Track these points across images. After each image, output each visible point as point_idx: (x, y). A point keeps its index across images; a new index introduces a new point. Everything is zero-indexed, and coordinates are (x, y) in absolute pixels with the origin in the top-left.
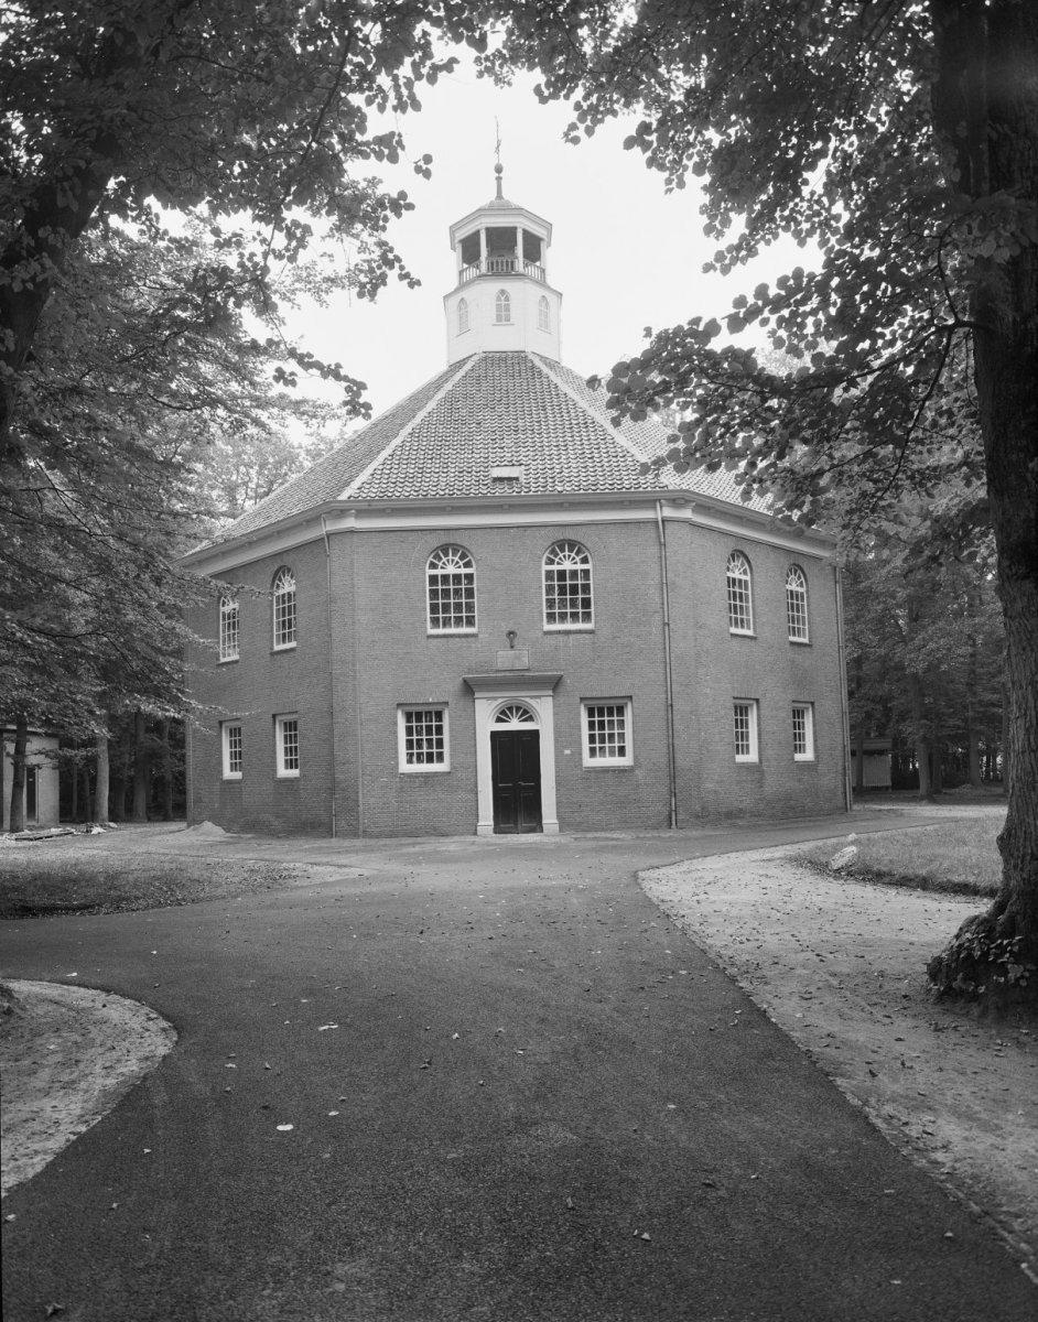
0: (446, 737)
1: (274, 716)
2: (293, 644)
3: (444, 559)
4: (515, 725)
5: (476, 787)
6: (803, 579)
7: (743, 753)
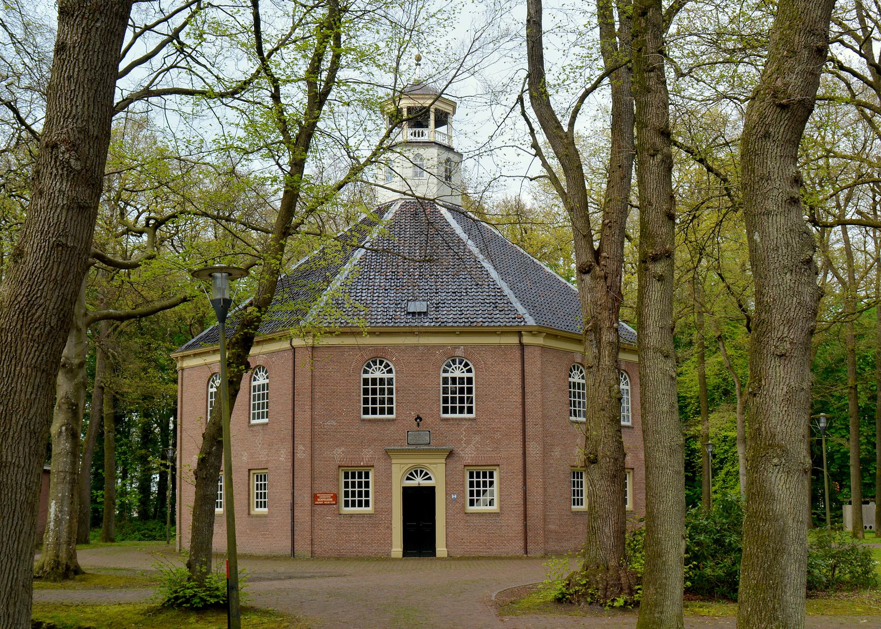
0: (371, 489)
1: (249, 470)
2: (266, 420)
3: (374, 367)
4: (418, 481)
6: (628, 379)
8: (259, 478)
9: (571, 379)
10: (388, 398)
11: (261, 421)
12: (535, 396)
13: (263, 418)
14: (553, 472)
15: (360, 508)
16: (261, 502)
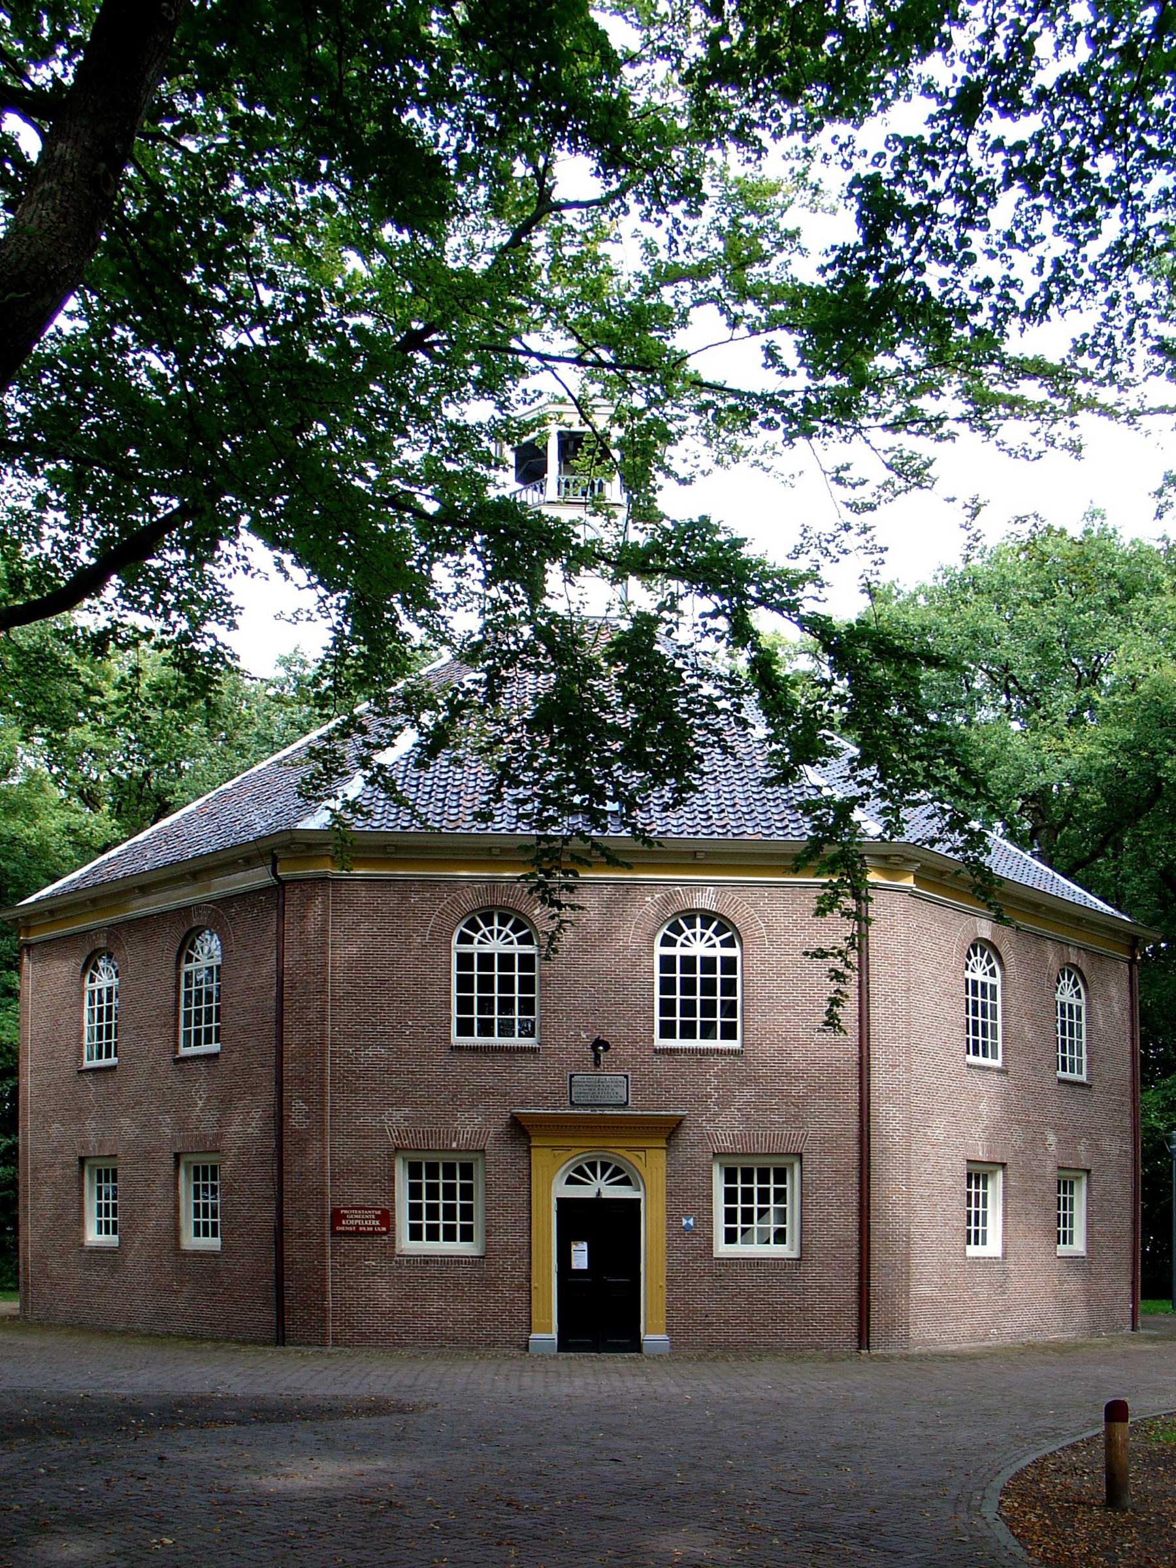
2: (214, 1047)
5: (530, 1281)
6: (1080, 986)
7: (976, 1243)
8: (200, 1172)
9: (969, 975)
10: (512, 1013)
11: (204, 1049)
12: (894, 1002)
13: (208, 1041)
14: (929, 1170)
15: (432, 1244)
16: (206, 1224)
